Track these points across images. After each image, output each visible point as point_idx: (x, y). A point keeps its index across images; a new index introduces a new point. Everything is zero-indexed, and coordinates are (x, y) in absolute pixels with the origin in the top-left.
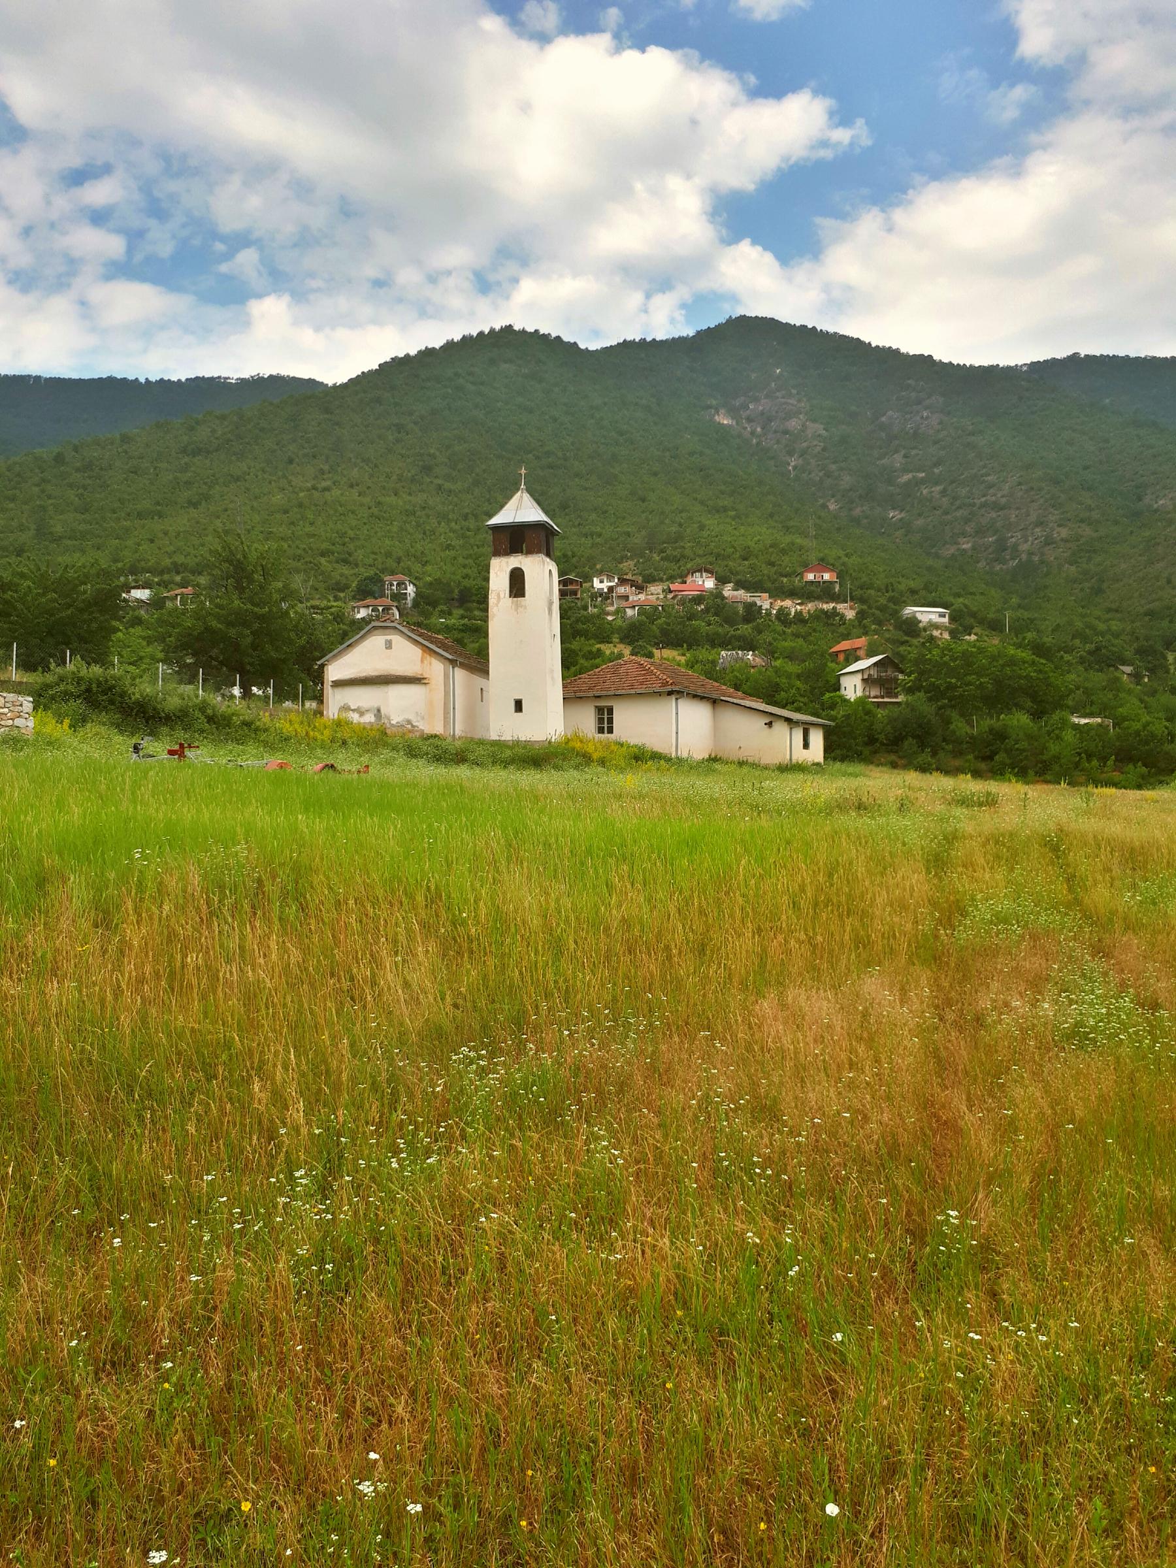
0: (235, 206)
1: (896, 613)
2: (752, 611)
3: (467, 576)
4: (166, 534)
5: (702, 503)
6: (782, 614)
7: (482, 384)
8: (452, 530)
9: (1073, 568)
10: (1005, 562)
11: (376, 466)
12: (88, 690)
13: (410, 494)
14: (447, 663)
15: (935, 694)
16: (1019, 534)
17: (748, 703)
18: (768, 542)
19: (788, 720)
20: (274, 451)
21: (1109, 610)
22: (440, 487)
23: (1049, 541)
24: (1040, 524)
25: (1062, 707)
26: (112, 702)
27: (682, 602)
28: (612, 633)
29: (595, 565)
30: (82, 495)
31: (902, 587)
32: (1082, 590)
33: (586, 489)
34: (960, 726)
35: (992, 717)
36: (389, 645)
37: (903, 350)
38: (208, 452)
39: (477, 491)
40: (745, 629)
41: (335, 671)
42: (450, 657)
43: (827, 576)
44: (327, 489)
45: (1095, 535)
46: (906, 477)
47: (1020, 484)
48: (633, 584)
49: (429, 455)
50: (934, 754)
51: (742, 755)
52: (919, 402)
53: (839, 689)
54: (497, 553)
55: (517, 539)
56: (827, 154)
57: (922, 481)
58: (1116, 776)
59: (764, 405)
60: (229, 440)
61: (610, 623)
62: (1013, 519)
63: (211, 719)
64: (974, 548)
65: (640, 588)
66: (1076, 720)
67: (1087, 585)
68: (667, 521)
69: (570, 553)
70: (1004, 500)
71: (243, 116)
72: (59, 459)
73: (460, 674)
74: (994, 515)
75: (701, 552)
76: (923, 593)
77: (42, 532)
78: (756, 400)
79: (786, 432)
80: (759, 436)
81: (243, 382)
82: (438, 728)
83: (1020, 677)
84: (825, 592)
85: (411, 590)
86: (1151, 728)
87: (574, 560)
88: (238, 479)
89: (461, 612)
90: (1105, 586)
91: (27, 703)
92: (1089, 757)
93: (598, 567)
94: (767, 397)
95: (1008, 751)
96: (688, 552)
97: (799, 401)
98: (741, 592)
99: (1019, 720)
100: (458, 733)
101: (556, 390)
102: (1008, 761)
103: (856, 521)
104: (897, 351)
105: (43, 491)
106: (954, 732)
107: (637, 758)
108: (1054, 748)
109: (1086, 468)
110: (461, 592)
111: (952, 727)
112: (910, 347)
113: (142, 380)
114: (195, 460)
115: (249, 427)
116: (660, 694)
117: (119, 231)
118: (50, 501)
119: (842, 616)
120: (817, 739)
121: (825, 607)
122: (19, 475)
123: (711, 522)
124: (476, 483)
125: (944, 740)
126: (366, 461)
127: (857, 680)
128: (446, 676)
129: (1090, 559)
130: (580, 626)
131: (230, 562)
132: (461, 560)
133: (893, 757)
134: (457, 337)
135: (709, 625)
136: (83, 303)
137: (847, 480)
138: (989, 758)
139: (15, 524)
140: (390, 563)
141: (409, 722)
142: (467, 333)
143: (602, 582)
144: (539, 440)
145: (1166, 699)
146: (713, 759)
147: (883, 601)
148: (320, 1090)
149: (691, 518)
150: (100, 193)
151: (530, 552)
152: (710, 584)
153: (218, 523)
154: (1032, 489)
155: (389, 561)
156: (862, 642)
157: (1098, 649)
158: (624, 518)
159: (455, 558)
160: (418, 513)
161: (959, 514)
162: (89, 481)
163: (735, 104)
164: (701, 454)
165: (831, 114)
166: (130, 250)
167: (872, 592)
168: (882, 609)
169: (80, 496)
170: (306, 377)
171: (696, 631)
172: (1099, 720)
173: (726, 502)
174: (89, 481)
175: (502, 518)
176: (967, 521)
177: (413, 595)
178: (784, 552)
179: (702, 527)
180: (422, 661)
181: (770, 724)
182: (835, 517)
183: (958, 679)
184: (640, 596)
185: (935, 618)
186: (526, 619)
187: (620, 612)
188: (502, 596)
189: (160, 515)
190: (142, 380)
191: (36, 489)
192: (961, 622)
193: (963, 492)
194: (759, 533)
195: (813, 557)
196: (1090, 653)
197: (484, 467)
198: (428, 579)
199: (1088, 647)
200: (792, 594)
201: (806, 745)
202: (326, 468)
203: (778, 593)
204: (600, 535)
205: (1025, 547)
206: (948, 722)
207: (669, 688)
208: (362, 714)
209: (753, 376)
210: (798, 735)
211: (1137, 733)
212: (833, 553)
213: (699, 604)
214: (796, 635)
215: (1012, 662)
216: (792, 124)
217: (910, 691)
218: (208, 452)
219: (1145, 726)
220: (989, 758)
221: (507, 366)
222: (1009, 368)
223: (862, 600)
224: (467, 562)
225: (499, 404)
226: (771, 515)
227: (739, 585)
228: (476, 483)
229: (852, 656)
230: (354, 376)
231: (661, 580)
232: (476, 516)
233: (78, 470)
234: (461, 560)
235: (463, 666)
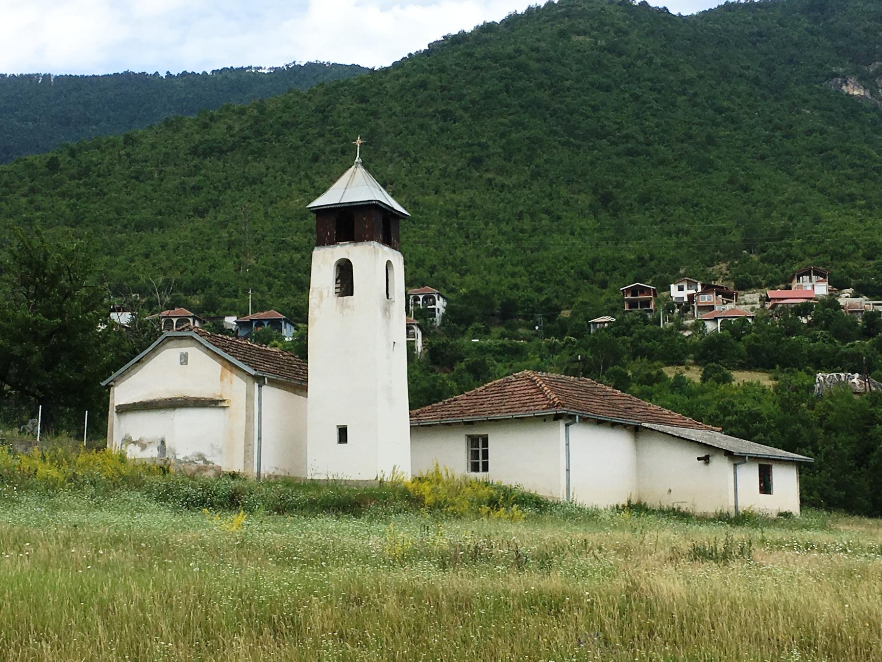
3: (516, 286)
4: (163, 247)
5: (822, 191)
7: (549, 60)
8: (501, 232)
11: (416, 161)
13: (454, 192)
14: (250, 380)
17: (686, 433)
19: (729, 454)
20: (297, 148)
22: (490, 181)
28: (686, 353)
29: (678, 269)
30: (75, 205)
33: (673, 178)
36: (184, 359)
38: (222, 152)
41: (123, 392)
42: (253, 373)
48: (719, 291)
49: (480, 145)
51: (668, 502)
55: (347, 223)
60: (245, 138)
61: (684, 340)
65: (728, 296)
68: (774, 214)
69: (647, 256)
72: (53, 165)
73: (272, 396)
75: (812, 250)
82: (237, 467)
85: (440, 304)
87: (652, 264)
88: (254, 182)
89: (502, 329)
93: (682, 271)
96: (795, 251)
100: (268, 468)
101: (639, 63)
105: (31, 202)
107: (493, 503)
110: (503, 305)
113: (163, 74)
114: (206, 162)
115: (271, 121)
116: (544, 419)
118: (38, 214)
123: (829, 214)
124: (535, 175)
126: (405, 155)
128: (249, 396)
130: (644, 344)
131: (30, 265)
132: (509, 268)
135: (815, 341)
141: (201, 457)
142: (533, 4)
143: (681, 289)
144: (616, 123)
149: (804, 210)
152: (821, 289)
155: (420, 271)
158: (719, 212)
159: (502, 265)
160: (462, 214)
162: (82, 189)
164: (822, 132)
169: (73, 207)
170: (349, 63)
173: (854, 188)
174: (82, 189)
175: (332, 196)
177: (442, 310)
179: (817, 220)
180: (222, 380)
181: (706, 460)
184: (728, 307)
187: (698, 326)
188: (325, 294)
189: (161, 225)
190: (163, 74)
191: (24, 200)
197: (545, 156)
198: (464, 290)
201: (766, 487)
204: (687, 233)
208: (144, 447)
210: (750, 475)
213: (805, 315)
218: (222, 152)
221: (581, 38)
224: (517, 269)
225: (568, 83)
228: (535, 175)
230: (399, 59)
231: (759, 286)
232: (532, 216)
233: (72, 177)
234: (509, 268)
235: (273, 383)
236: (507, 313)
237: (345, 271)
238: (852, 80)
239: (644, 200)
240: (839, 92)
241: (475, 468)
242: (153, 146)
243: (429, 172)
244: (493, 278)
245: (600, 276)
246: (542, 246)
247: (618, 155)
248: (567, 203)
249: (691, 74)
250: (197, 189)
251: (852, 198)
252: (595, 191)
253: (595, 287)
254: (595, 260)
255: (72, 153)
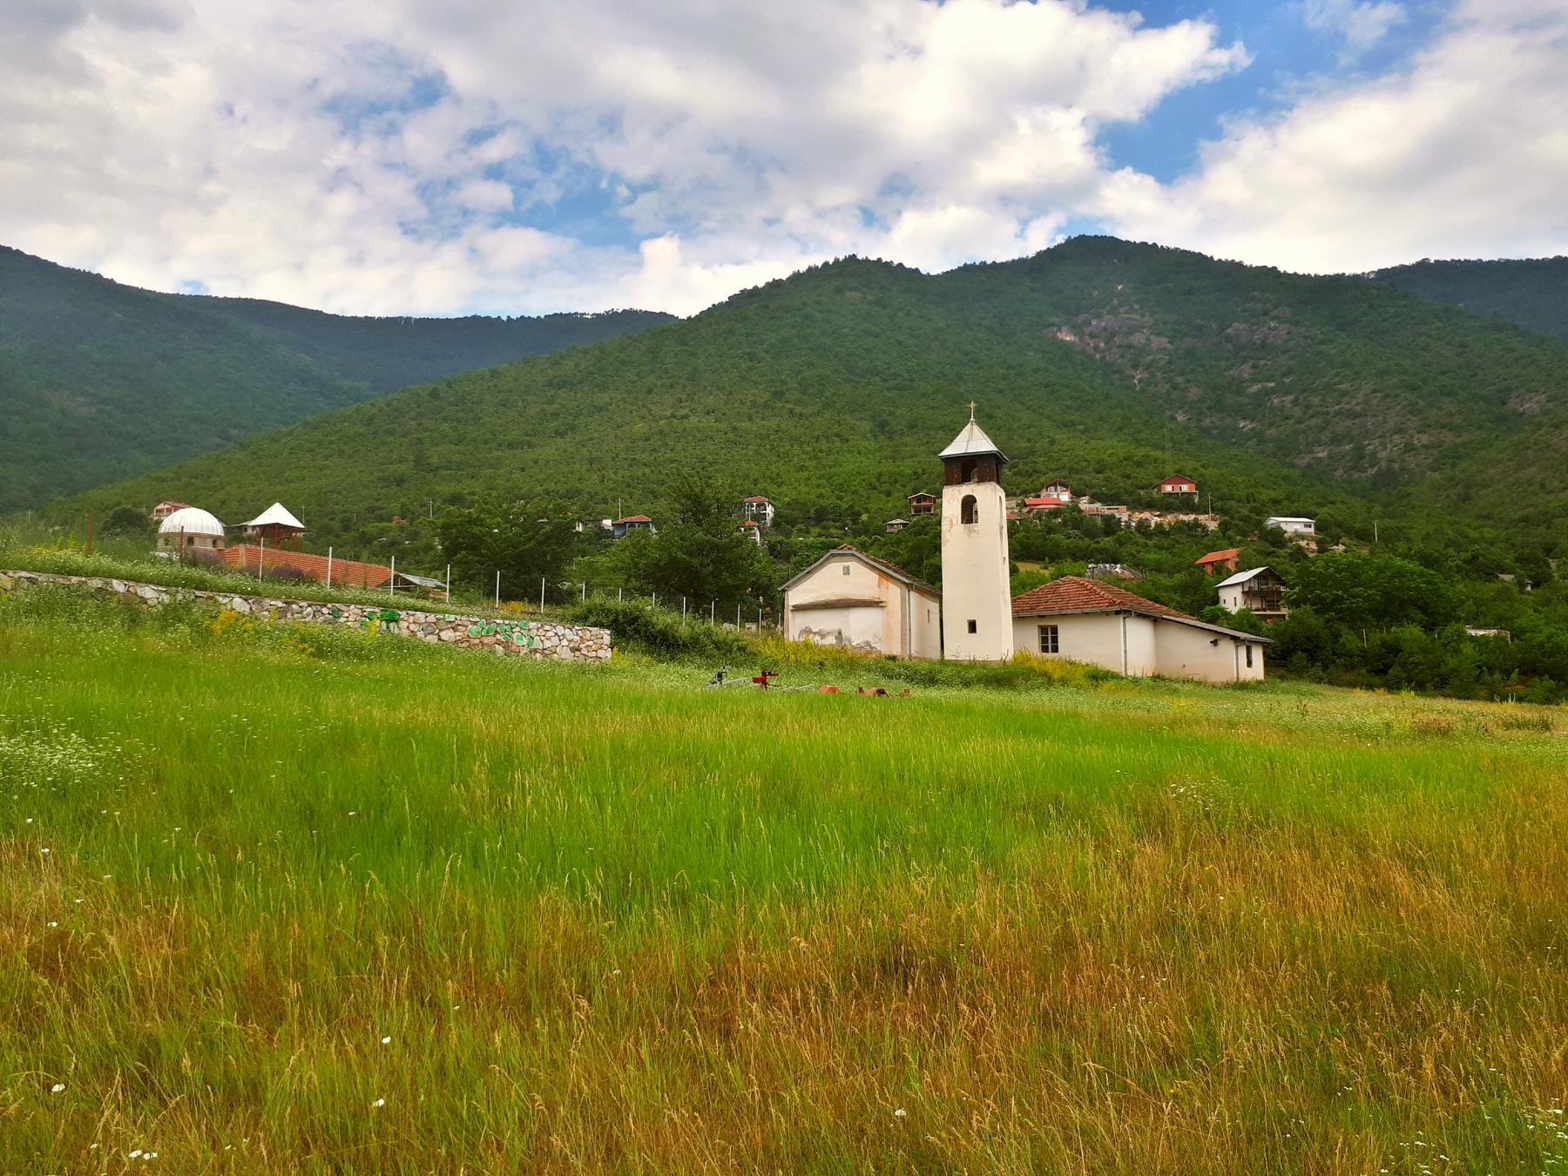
0: (630, 159)
1: (1259, 524)
2: (1111, 525)
3: (821, 496)
4: (536, 462)
5: (1049, 418)
6: (1143, 526)
9: (1436, 475)
10: (1363, 470)
12: (616, 621)
15: (1322, 606)
16: (1377, 442)
18: (1122, 454)
19: (1234, 638)
21: (1479, 517)
22: (791, 411)
23: (1409, 448)
24: (1398, 431)
25: (1459, 620)
26: (637, 631)
27: (1039, 516)
31: (1264, 497)
32: (1448, 496)
34: (1349, 640)
35: (1381, 630)
36: (847, 571)
37: (1247, 263)
39: (827, 414)
40: (1107, 542)
41: (795, 596)
43: (1185, 488)
44: (686, 417)
45: (1458, 441)
46: (1255, 388)
47: (1374, 391)
50: (1325, 667)
52: (1265, 313)
53: (1217, 602)
54: (950, 483)
55: (968, 468)
56: (1207, 76)
57: (1273, 391)
58: (1522, 690)
59: (1107, 321)
62: (1370, 426)
63: (717, 645)
64: (1330, 457)
66: (1473, 632)
67: (1452, 492)
70: (1358, 408)
71: (649, 74)
72: (434, 394)
74: (1349, 422)
76: (1286, 503)
77: (419, 463)
78: (1099, 316)
79: (1130, 347)
80: (1102, 351)
81: (598, 317)
82: (896, 650)
83: (1409, 589)
84: (1185, 504)
85: (770, 510)
86: (1556, 640)
89: (817, 530)
90: (1472, 492)
91: (606, 636)
92: (1491, 670)
94: (1109, 313)
95: (1403, 665)
96: (1040, 467)
97: (1143, 316)
98: (1098, 505)
99: (1411, 632)
102: (1404, 675)
103: (1206, 432)
104: (1240, 264)
106: (1344, 645)
108: (1452, 662)
109: (1444, 373)
111: (1342, 640)
112: (1253, 259)
117: (511, 182)
119: (1204, 527)
120: (1258, 655)
121: (1185, 518)
122: (397, 410)
124: (826, 406)
125: (1334, 653)
126: (722, 389)
127: (1237, 593)
128: (903, 599)
129: (1453, 465)
131: (688, 497)
132: (814, 480)
133: (1282, 671)
134: (803, 269)
136: (473, 251)
137: (1194, 392)
138: (1383, 671)
139: (395, 456)
140: (748, 485)
141: (868, 644)
145: (1562, 609)
146: (1157, 678)
147: (1245, 512)
148: (1463, 1010)
150: (494, 151)
151: (981, 480)
152: (1065, 497)
153: (584, 451)
154: (1388, 396)
156: (1231, 553)
157: (1475, 557)
161: (1313, 422)
163: (1212, 49)
165: (1212, 38)
166: (518, 200)
167: (1233, 503)
168: (1246, 520)
171: (1057, 545)
172: (1493, 632)
175: (955, 448)
176: (1321, 429)
178: (1138, 464)
179: (1052, 442)
181: (1215, 643)
182: (1186, 429)
183: (1345, 591)
185: (1301, 528)
186: (977, 543)
189: (530, 445)
192: (1327, 531)
193: (1316, 400)
194: (1112, 447)
195: (1169, 470)
196: (1465, 561)
199: (1463, 555)
200: (1150, 506)
201: (1249, 664)
202: (684, 396)
203: (1136, 505)
205: (1383, 455)
206: (1337, 636)
207: (1117, 608)
208: (823, 636)
209: (1095, 293)
210: (1243, 652)
211: (1541, 645)
212: (1189, 465)
214: (1160, 548)
215: (1400, 573)
216: (1180, 51)
217: (1294, 604)
219: (1549, 637)
220: (1383, 671)
222: (1356, 277)
223: (1223, 512)
226: (1120, 429)
227: (1095, 498)
228: (826, 406)
229: (1221, 570)
232: (827, 438)
233: (451, 404)
236: (820, 517)
237: (969, 506)
238: (1065, 328)
239: (912, 426)
240: (1054, 337)
241: (1045, 649)
242: (515, 379)
243: (742, 403)
244: (803, 489)
245: (886, 487)
246: (837, 463)
247: (889, 389)
248: (852, 429)
249: (941, 324)
250: (556, 414)
251: (1073, 424)
252: (873, 418)
253: (883, 496)
254: (880, 474)
255: (449, 385)
